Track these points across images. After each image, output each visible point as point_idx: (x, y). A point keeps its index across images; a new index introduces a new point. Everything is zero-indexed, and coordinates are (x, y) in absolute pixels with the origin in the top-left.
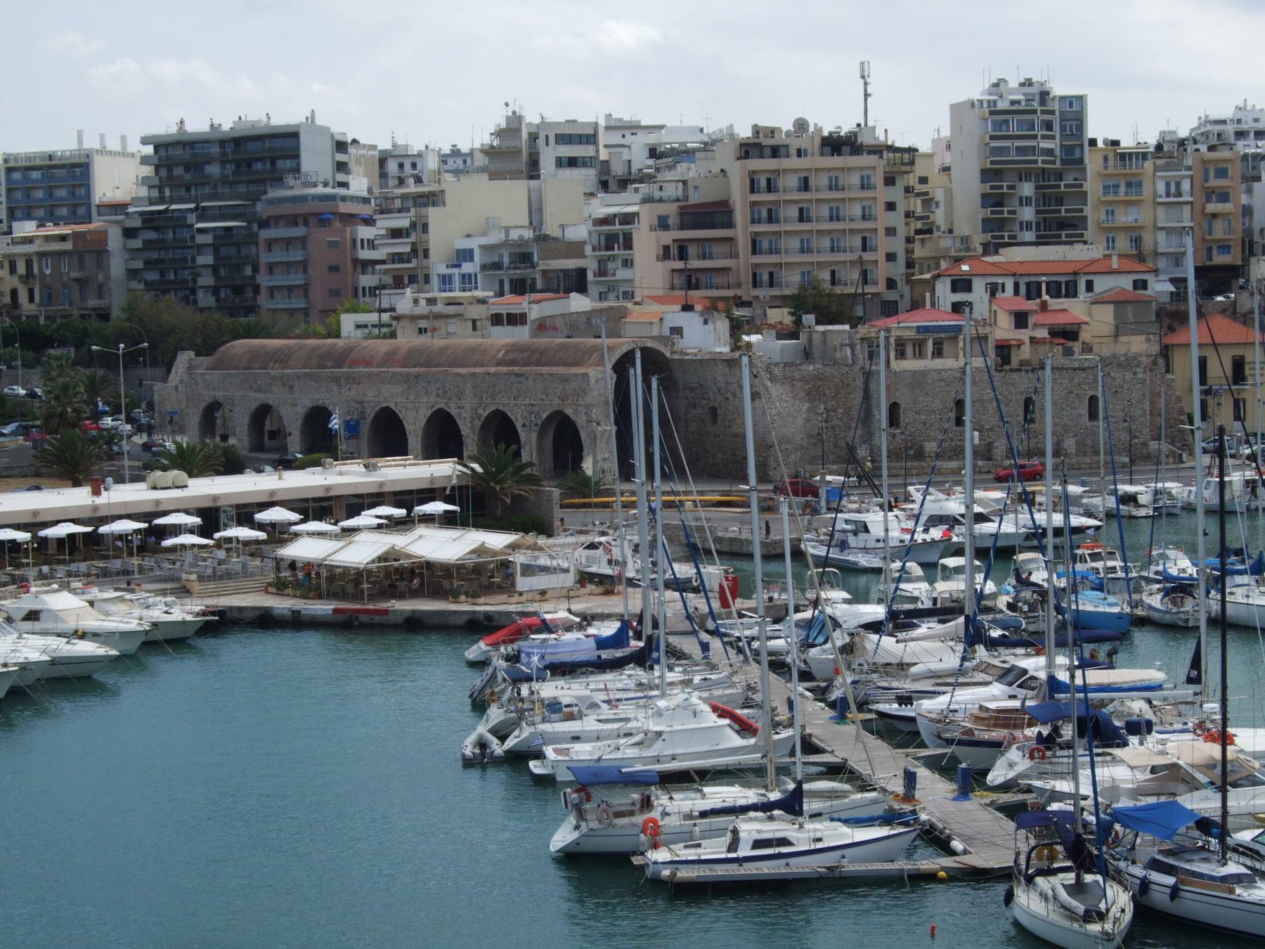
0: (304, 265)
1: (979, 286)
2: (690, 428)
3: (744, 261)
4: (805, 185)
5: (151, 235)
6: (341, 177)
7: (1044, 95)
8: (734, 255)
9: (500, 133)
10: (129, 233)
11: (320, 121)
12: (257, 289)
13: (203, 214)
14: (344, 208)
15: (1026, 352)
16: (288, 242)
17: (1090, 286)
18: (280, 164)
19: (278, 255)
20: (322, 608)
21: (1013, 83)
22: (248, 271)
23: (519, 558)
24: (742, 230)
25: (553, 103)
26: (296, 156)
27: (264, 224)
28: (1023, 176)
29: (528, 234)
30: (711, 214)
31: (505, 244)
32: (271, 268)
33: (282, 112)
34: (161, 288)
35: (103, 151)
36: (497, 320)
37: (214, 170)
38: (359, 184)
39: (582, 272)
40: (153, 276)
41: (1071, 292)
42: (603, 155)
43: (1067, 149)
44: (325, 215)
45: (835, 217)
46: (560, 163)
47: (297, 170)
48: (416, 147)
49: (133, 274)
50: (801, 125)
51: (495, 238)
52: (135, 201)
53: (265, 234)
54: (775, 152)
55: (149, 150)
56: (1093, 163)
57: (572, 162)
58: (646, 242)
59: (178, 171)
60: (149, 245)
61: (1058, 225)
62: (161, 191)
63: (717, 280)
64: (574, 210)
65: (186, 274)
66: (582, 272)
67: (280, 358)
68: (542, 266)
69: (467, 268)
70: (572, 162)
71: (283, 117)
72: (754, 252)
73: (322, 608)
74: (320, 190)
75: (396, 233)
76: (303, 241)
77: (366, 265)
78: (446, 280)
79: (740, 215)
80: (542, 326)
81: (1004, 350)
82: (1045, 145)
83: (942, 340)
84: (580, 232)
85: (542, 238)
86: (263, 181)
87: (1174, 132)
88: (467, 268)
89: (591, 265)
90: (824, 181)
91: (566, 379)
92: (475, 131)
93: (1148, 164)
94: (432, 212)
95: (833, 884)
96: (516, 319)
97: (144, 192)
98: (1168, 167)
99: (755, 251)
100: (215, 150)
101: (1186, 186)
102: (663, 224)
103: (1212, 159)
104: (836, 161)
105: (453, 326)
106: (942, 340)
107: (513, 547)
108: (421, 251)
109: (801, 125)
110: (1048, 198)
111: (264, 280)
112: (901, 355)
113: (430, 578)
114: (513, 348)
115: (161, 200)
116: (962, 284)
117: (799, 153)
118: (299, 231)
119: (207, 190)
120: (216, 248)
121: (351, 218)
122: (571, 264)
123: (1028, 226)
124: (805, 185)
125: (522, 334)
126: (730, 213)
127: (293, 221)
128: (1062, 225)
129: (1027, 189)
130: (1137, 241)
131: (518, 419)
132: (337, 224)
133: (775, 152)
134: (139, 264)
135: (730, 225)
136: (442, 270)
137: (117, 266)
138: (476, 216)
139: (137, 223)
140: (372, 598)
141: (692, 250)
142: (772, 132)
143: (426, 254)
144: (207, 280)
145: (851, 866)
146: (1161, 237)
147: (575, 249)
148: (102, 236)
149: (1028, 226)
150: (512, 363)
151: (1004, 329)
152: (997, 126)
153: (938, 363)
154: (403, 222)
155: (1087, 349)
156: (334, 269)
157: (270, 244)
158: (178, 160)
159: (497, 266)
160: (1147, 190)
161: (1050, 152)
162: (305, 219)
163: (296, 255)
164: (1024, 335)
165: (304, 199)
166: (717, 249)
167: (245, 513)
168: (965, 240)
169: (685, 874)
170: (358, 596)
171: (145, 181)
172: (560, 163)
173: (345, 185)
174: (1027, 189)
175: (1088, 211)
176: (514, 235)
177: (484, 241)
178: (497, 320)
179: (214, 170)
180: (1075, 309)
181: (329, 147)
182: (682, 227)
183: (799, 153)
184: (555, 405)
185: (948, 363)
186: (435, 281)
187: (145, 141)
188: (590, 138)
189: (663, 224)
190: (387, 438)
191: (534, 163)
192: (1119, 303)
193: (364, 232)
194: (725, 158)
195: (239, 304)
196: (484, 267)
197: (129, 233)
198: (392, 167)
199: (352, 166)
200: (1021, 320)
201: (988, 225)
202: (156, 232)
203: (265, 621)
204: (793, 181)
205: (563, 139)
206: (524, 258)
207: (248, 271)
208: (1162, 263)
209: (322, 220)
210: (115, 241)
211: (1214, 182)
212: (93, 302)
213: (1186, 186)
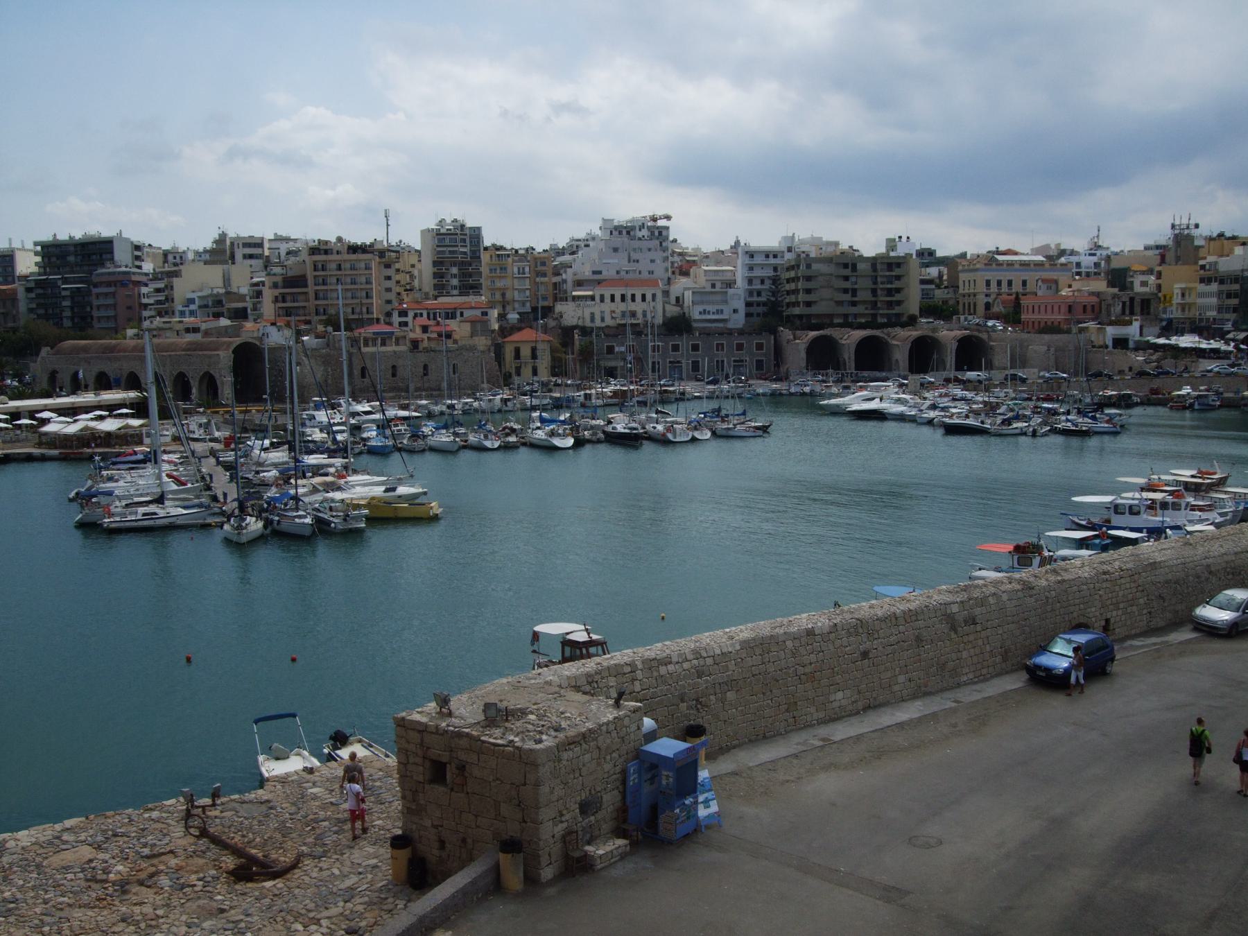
0: (114, 306)
1: (411, 314)
2: (254, 375)
3: (312, 303)
4: (339, 268)
5: (40, 291)
6: (137, 263)
7: (463, 226)
8: (307, 300)
9: (216, 242)
10: (29, 290)
11: (124, 235)
12: (92, 317)
13: (66, 281)
14: (134, 278)
15: (425, 344)
16: (106, 295)
17: (462, 314)
18: (104, 256)
19: (102, 301)
20: (55, 452)
21: (449, 221)
22: (88, 309)
23: (144, 430)
24: (311, 289)
25: (241, 228)
26: (112, 253)
27: (96, 286)
28: (454, 264)
29: (222, 291)
30: (294, 281)
31: (211, 295)
32: (99, 307)
33: (106, 231)
34: (47, 317)
35: (23, 249)
36: (188, 330)
37: (71, 259)
38: (148, 267)
39: (245, 309)
40: (41, 311)
41: (453, 317)
42: (267, 253)
43: (473, 252)
44: (124, 281)
45: (354, 282)
46: (246, 257)
47: (112, 259)
48: (182, 248)
49: (31, 310)
50: (340, 239)
51: (206, 292)
52: (32, 274)
53: (95, 291)
54: (326, 252)
55: (39, 248)
56: (485, 257)
57: (251, 257)
58: (268, 294)
59: (54, 259)
60: (38, 296)
61: (469, 286)
62: (45, 268)
63: (301, 312)
64: (243, 277)
65: (58, 311)
66: (245, 309)
67: (85, 349)
68: (227, 306)
69: (192, 307)
70: (251, 257)
71: (106, 233)
72: (316, 298)
73: (55, 452)
74: (123, 269)
75: (158, 290)
76: (114, 294)
77: (146, 306)
78: (182, 314)
79: (310, 282)
80: (207, 333)
81: (415, 344)
82: (462, 250)
83: (385, 339)
84: (244, 290)
85: (228, 293)
86: (95, 265)
87: (837, 244)
88: (192, 307)
89: (249, 305)
90: (348, 266)
91: (210, 357)
92: (205, 242)
93: (510, 260)
94: (175, 280)
95: (172, 527)
96: (196, 330)
97: (36, 269)
98: (520, 261)
99: (316, 298)
100: (72, 249)
101: (527, 269)
102: (275, 286)
103: (1236, 260)
104: (353, 257)
105: (168, 334)
106: (385, 339)
107: (141, 426)
108: (169, 299)
109: (340, 239)
110: (464, 275)
111: (95, 314)
112: (366, 345)
113: (108, 439)
114: (190, 343)
115: (45, 274)
116: (403, 313)
117: (338, 253)
118: (112, 289)
119: (67, 269)
120: (72, 297)
121: (139, 284)
122: (240, 305)
123: (455, 288)
124: (339, 268)
125: (197, 337)
126: (306, 281)
127: (109, 284)
128: (472, 287)
129: (455, 270)
130: (503, 295)
131: (190, 375)
132: (131, 286)
133: (326, 252)
134: (34, 306)
135: (306, 286)
136: (180, 308)
137: (23, 306)
138: (198, 282)
139: (32, 285)
140: (78, 448)
141: (288, 298)
142: (326, 242)
143: (173, 301)
144: (68, 313)
145: (180, 522)
146: (516, 293)
147: (242, 298)
148: (14, 292)
149: (455, 288)
150: (189, 350)
151: (417, 334)
152: (439, 240)
153: (383, 349)
154: (161, 285)
155: (455, 342)
156: (129, 308)
157: (98, 296)
158: (54, 253)
159: (206, 306)
160: (509, 270)
161: (465, 253)
162: (114, 284)
163: (110, 301)
164: (425, 336)
165: (114, 273)
166: (301, 297)
167: (31, 414)
168: (426, 294)
169: (113, 525)
170: (71, 447)
171: (37, 264)
172: (246, 257)
173: (140, 267)
174: (455, 270)
175: (482, 281)
176: (215, 292)
177: (200, 294)
178: (188, 330)
179: (71, 259)
180: (453, 325)
181: (129, 248)
182: (284, 287)
183: (338, 253)
184: (206, 369)
185: (388, 349)
186: (177, 314)
187: (36, 244)
188: (259, 244)
189: (275, 286)
190: (103, 383)
191: (233, 257)
192: (473, 322)
193: (144, 290)
194: (304, 256)
195: (83, 324)
196: (200, 307)
197: (29, 290)
198: (170, 258)
199: (144, 257)
200: (425, 329)
201: (436, 287)
202: (40, 287)
203: (29, 458)
204: (334, 266)
205: (246, 245)
206: (219, 303)
207: (88, 309)
208: (516, 305)
209: (123, 284)
210: (21, 294)
211: (540, 268)
212: (10, 325)
213: (527, 269)
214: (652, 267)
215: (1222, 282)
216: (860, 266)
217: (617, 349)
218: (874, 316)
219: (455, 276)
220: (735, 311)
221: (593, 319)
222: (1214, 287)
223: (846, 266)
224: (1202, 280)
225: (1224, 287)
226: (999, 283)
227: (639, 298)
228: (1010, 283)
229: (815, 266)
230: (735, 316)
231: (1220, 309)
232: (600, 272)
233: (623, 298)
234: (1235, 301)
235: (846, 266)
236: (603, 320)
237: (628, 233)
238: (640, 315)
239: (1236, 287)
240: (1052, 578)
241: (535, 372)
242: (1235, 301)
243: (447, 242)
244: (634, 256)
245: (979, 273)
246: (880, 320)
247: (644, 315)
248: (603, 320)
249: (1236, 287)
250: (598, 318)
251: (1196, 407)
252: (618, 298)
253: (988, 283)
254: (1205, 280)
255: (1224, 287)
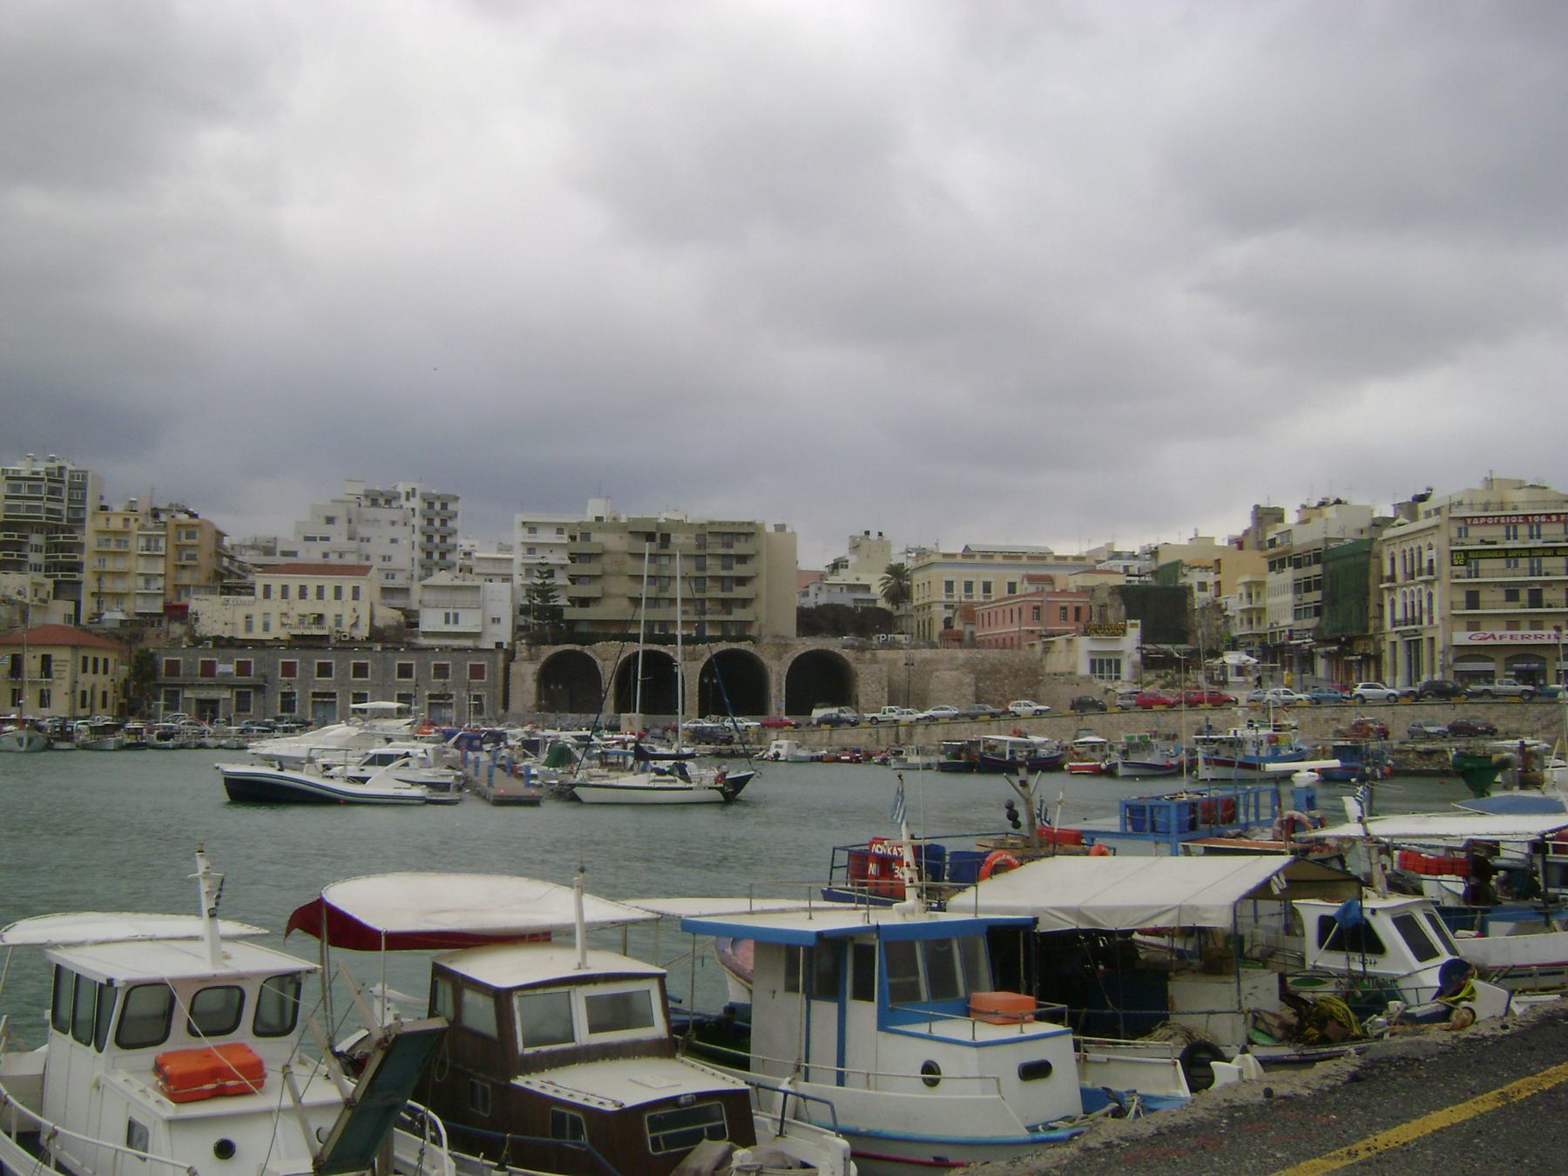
129: (36, 539)
214: (390, 550)
215: (1297, 563)
216: (678, 539)
217: (221, 668)
218: (701, 626)
219: (37, 549)
220: (496, 620)
221: (249, 627)
222: (1289, 574)
223: (650, 537)
224: (1272, 567)
225: (1302, 573)
226: (969, 586)
227: (329, 593)
228: (987, 588)
229: (596, 537)
230: (495, 628)
231: (1297, 613)
232: (294, 554)
233: (303, 593)
234: (1315, 596)
235: (650, 537)
236: (266, 627)
237: (388, 502)
238: (330, 622)
239: (1316, 569)
240: (1353, 1148)
241: (44, 700)
242: (1315, 596)
243: (24, 492)
244: (363, 531)
245: (935, 570)
246: (709, 632)
247: (338, 622)
248: (266, 627)
249: (1316, 569)
250: (258, 623)
251: (1121, 771)
252: (294, 592)
253: (949, 586)
254: (1276, 564)
255: (1302, 573)
